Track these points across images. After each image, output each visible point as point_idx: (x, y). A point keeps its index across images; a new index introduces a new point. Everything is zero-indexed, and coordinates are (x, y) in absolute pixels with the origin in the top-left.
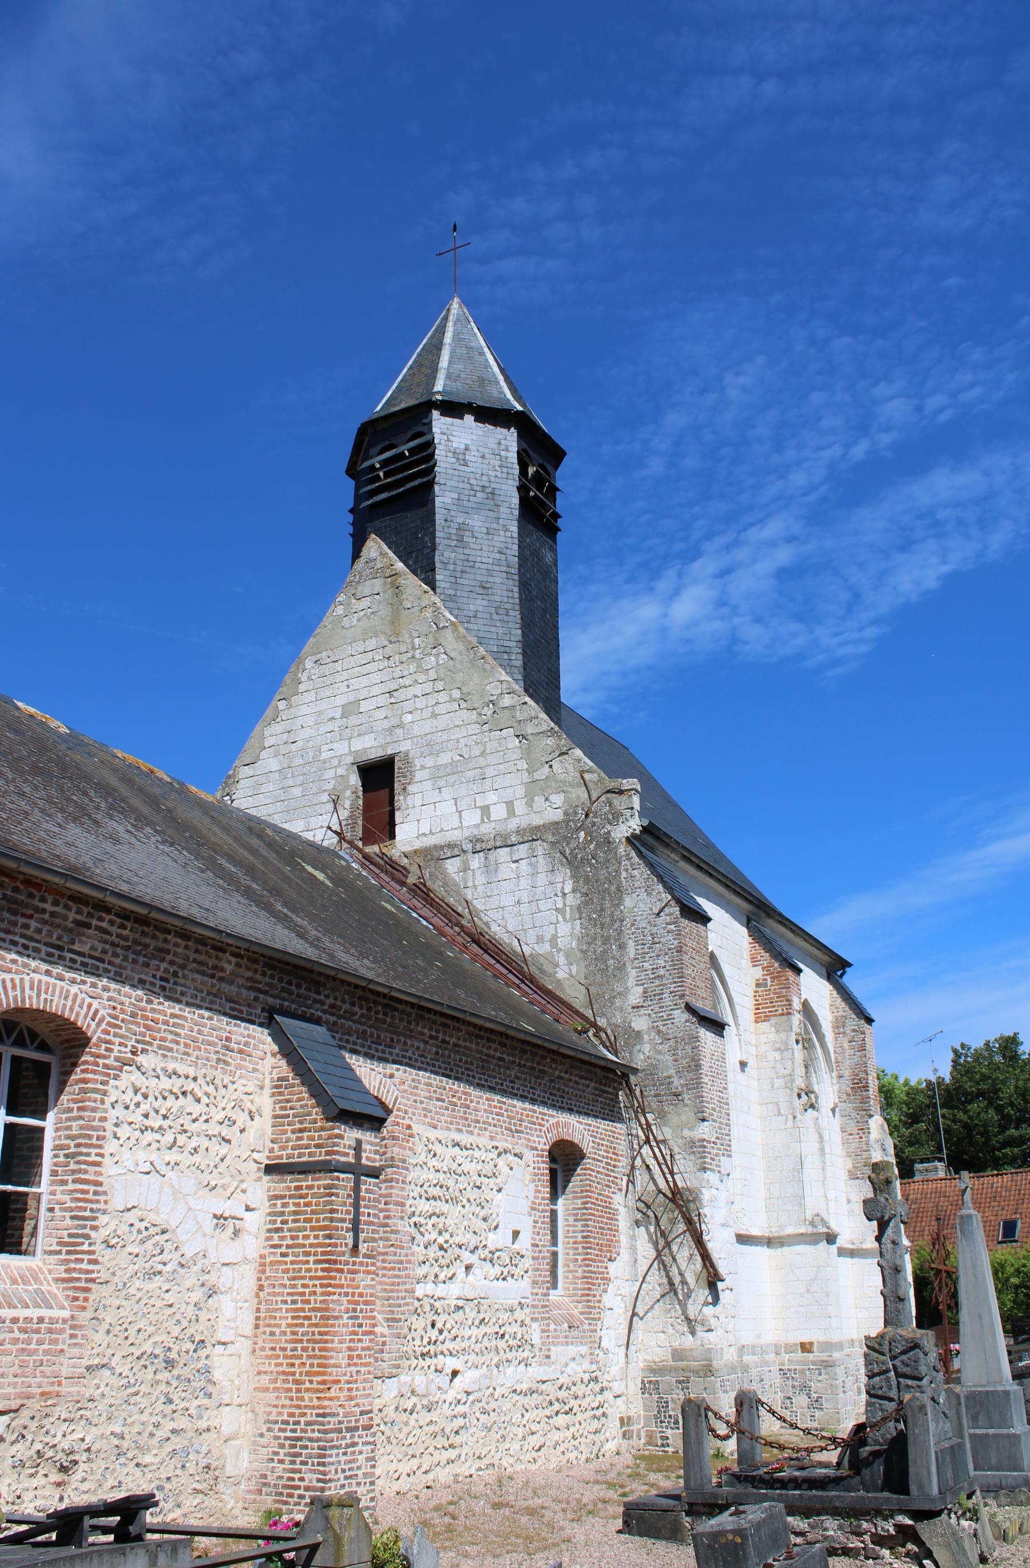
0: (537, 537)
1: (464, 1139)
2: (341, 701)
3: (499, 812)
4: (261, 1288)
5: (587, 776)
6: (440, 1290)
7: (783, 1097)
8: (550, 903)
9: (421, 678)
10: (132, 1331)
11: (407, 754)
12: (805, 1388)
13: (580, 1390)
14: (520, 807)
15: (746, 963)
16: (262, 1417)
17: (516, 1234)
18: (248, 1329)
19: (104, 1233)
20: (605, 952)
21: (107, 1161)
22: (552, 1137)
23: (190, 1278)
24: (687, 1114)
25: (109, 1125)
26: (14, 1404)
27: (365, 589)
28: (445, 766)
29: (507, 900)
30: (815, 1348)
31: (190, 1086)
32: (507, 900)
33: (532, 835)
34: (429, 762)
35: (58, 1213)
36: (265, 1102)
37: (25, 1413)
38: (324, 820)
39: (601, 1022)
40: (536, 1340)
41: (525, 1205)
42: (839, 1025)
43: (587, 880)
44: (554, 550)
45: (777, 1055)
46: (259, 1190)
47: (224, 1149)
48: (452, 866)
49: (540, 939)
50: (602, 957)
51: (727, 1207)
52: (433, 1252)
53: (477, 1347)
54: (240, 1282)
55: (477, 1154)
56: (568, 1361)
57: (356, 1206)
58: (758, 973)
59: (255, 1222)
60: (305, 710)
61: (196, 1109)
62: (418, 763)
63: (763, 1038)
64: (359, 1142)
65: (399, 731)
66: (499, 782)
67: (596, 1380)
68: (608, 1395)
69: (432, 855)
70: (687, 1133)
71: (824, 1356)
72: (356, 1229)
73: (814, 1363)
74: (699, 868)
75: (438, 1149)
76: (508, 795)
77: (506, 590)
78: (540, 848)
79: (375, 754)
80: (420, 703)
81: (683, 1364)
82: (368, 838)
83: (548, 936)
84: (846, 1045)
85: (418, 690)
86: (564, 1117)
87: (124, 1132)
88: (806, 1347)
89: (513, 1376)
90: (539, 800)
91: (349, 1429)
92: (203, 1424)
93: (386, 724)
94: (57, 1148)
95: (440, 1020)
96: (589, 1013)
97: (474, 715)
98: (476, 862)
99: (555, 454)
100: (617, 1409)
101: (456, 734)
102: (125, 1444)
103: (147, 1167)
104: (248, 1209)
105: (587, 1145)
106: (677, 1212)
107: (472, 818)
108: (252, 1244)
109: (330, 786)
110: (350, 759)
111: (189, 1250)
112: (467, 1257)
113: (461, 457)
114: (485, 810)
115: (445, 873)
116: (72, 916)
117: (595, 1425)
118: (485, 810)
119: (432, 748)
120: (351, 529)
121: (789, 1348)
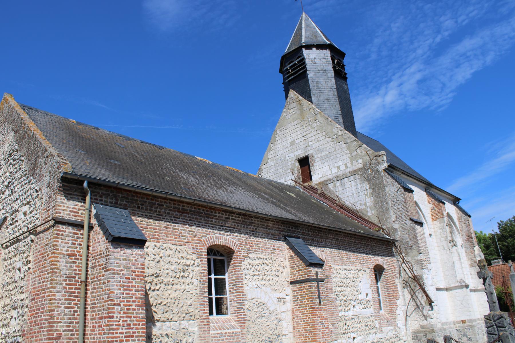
1: (347, 267)
2: (289, 141)
3: (343, 167)
4: (294, 318)
6: (346, 314)
7: (445, 243)
11: (312, 154)
12: (465, 334)
14: (349, 165)
15: (427, 203)
17: (367, 295)
19: (247, 306)
20: (382, 205)
21: (245, 285)
22: (374, 264)
23: (273, 317)
24: (415, 252)
25: (243, 275)
27: (291, 106)
29: (349, 194)
30: (467, 322)
31: (265, 261)
32: (349, 194)
33: (354, 173)
34: (319, 155)
35: (233, 302)
36: (287, 263)
39: (384, 227)
40: (377, 326)
41: (368, 286)
42: (460, 219)
43: (373, 184)
45: (441, 231)
46: (289, 289)
47: (277, 279)
50: (381, 207)
52: (343, 303)
54: (288, 316)
55: (352, 272)
57: (319, 291)
58: (431, 206)
59: (289, 299)
60: (279, 145)
61: (268, 268)
62: (316, 156)
63: (436, 226)
64: (317, 272)
67: (397, 337)
69: (325, 183)
70: (416, 258)
71: (470, 324)
72: (319, 298)
73: (467, 326)
75: (340, 271)
76: (345, 162)
77: (334, 100)
78: (357, 176)
79: (302, 155)
80: (314, 138)
82: (304, 181)
83: (363, 203)
84: (463, 225)
85: (312, 134)
86: (377, 258)
87: (248, 277)
88: (463, 322)
93: (304, 146)
94: (230, 283)
97: (330, 139)
98: (338, 184)
101: (326, 146)
103: (256, 286)
105: (385, 265)
107: (335, 170)
109: (290, 167)
110: (295, 158)
111: (271, 309)
112: (353, 303)
113: (314, 61)
114: (338, 168)
115: (329, 188)
116: (224, 216)
118: (338, 168)
119: (319, 151)
120: (284, 89)
121: (458, 322)
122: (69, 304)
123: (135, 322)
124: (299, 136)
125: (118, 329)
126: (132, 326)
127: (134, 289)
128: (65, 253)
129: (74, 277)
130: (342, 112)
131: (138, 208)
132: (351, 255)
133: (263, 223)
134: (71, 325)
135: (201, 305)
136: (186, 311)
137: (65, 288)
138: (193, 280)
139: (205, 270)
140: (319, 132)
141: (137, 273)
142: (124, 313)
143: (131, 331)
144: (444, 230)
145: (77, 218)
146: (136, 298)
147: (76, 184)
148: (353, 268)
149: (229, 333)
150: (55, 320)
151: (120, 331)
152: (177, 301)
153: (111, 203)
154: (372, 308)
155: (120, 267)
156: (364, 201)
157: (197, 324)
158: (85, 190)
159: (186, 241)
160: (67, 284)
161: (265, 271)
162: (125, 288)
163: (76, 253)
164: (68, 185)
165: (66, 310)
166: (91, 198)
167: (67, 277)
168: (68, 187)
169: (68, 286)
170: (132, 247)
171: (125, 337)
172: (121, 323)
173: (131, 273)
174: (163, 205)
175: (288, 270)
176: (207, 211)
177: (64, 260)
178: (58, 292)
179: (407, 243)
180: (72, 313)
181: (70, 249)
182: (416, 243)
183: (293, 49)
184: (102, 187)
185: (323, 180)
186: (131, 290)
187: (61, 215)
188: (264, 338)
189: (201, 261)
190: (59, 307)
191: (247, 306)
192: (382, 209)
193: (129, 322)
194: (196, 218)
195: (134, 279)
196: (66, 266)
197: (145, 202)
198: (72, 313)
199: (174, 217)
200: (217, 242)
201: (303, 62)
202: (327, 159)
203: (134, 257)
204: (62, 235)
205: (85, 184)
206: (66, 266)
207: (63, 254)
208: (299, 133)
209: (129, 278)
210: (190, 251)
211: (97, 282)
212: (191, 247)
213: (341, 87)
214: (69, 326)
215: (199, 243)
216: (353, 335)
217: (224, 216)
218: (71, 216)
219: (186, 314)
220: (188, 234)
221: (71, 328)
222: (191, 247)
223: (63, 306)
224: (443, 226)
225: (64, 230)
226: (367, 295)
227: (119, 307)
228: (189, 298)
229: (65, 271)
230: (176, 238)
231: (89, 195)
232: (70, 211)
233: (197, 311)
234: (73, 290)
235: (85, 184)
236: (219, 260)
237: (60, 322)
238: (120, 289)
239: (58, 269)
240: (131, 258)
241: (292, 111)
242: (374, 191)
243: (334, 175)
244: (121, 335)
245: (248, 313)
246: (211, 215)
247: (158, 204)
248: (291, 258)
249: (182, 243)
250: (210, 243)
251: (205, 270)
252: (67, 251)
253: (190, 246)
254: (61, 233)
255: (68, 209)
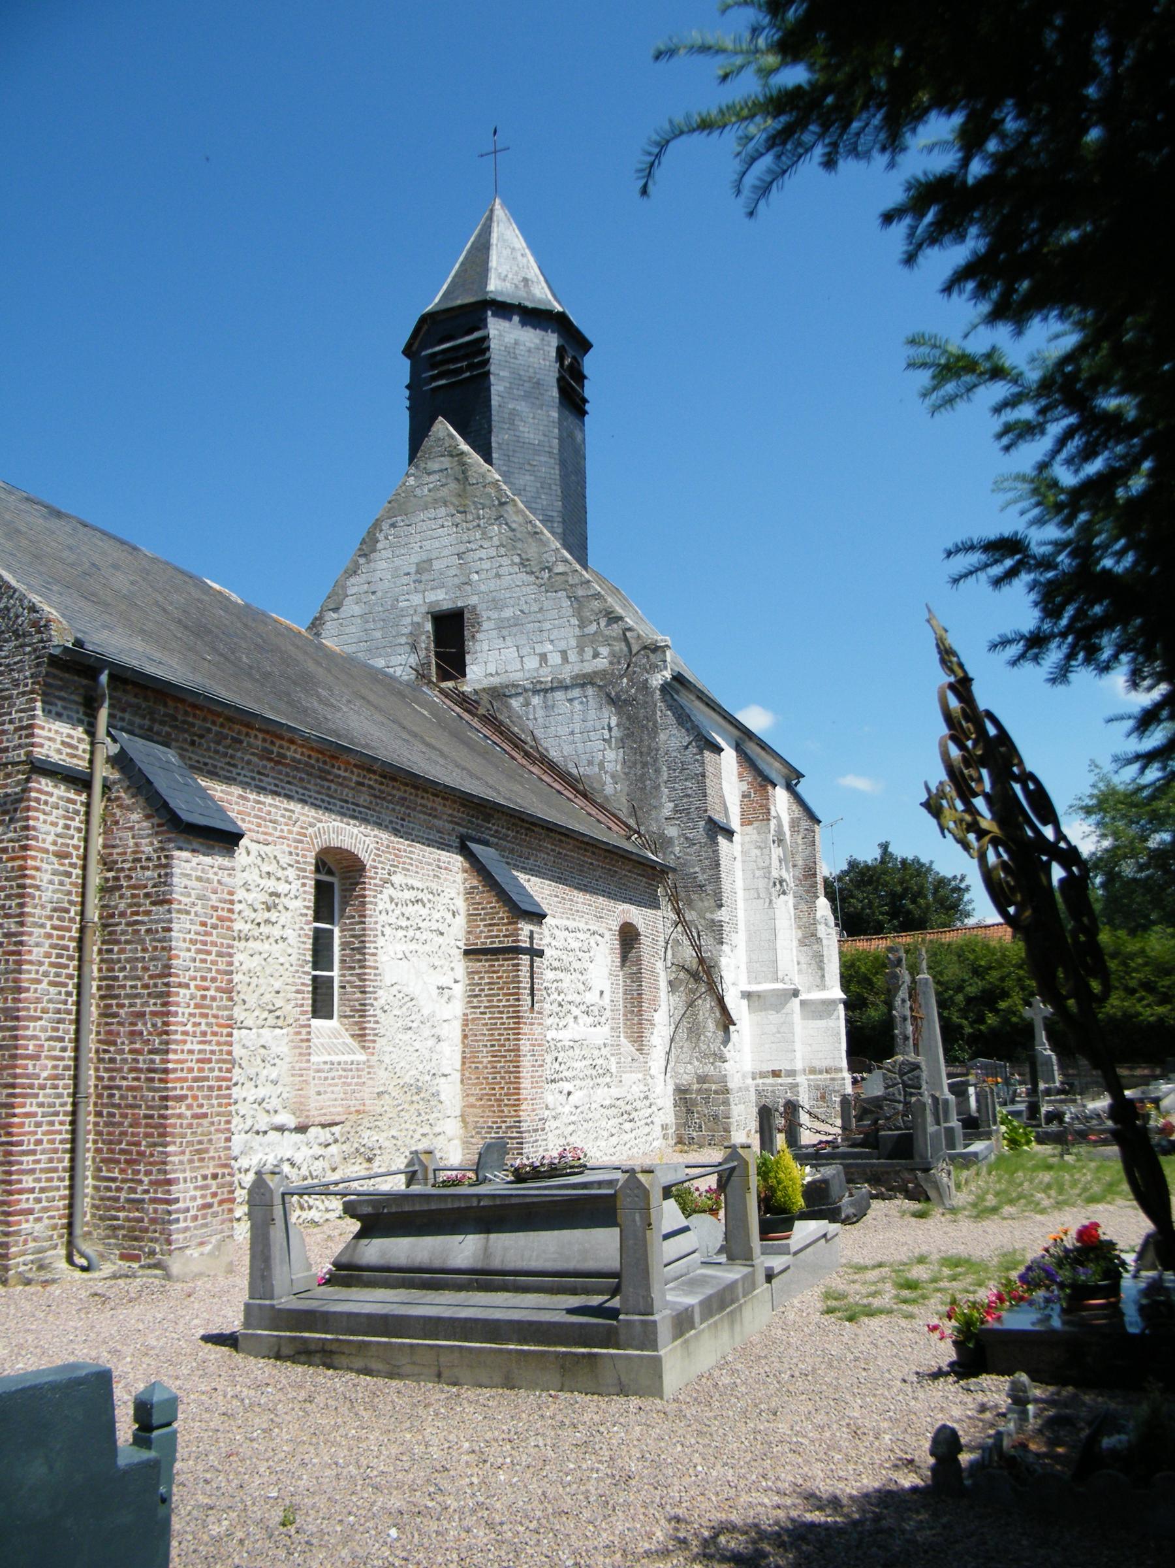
0: (571, 420)
1: (571, 924)
2: (415, 559)
3: (555, 659)
4: (465, 1036)
5: (628, 634)
6: (560, 1035)
7: (762, 884)
8: (598, 735)
9: (486, 544)
10: (398, 1067)
11: (474, 607)
13: (638, 1104)
14: (573, 656)
15: (734, 778)
16: (471, 1126)
17: (602, 993)
18: (458, 1066)
19: (382, 1001)
20: (643, 775)
21: (380, 952)
22: (621, 920)
23: (426, 1032)
24: (709, 903)
25: (379, 927)
26: (342, 1118)
27: (434, 465)
28: (508, 619)
29: (563, 730)
31: (420, 895)
32: (563, 730)
33: (584, 681)
34: (494, 615)
35: (349, 989)
36: (461, 904)
37: (348, 1124)
38: (402, 659)
39: (643, 830)
40: (614, 1070)
41: (606, 971)
42: (794, 824)
43: (629, 718)
44: (583, 431)
45: (758, 852)
46: (460, 966)
47: (440, 939)
48: (515, 703)
49: (590, 763)
50: (642, 779)
51: (735, 972)
52: (555, 1008)
53: (581, 1075)
54: (453, 1032)
55: (579, 935)
56: (631, 1085)
57: (532, 978)
58: (745, 787)
59: (459, 990)
60: (383, 565)
61: (424, 912)
62: (485, 615)
63: (747, 838)
64: (532, 932)
65: (468, 588)
66: (555, 634)
67: (646, 1098)
68: (654, 1108)
69: (499, 694)
70: (708, 915)
72: (532, 994)
74: (708, 705)
75: (556, 931)
76: (563, 645)
77: (549, 468)
78: (590, 691)
79: (447, 605)
80: (486, 565)
81: (705, 1086)
82: (444, 676)
83: (597, 761)
84: (800, 841)
85: (482, 553)
86: (626, 906)
87: (387, 930)
88: (776, 1074)
89: (603, 1095)
90: (589, 652)
91: (536, 1131)
92: (437, 1130)
93: (457, 581)
94: (342, 944)
95: (558, 837)
96: (632, 822)
97: (532, 579)
98: (536, 700)
99: (584, 345)
100: (659, 1119)
101: (518, 592)
102: (399, 1143)
103: (401, 955)
104: (456, 982)
105: (641, 928)
106: (702, 976)
107: (532, 663)
108: (457, 1008)
109: (406, 631)
110: (424, 609)
111: (426, 1012)
112: (576, 1011)
113: (511, 351)
114: (543, 657)
115: (509, 707)
116: (354, 778)
117: (647, 1129)
118: (543, 657)
119: (497, 604)
120: (407, 403)
121: (763, 1075)
122: (58, 975)
123: (215, 1029)
124: (446, 552)
125: (185, 1042)
126: (209, 1038)
127: (214, 949)
128: (52, 848)
129: (67, 911)
130: (564, 506)
131: (193, 743)
132: (580, 897)
133: (424, 802)
134: (61, 1026)
135: (298, 992)
136: (271, 1007)
137: (50, 936)
138: (288, 933)
139: (308, 908)
140: (502, 551)
141: (220, 913)
142: (197, 1006)
143: (208, 1047)
144: (766, 851)
145: (75, 761)
146: (218, 971)
147: (79, 673)
148: (582, 926)
149: (346, 1063)
150: (32, 1013)
151: (188, 1046)
152: (254, 981)
153: (141, 727)
154: (606, 1028)
155: (189, 895)
156: (600, 756)
157: (286, 1040)
158: (99, 692)
159: (278, 834)
160: (54, 928)
161: (419, 920)
162: (199, 946)
163: (71, 849)
164: (61, 675)
165: (52, 989)
166: (111, 716)
167: (55, 910)
168: (61, 679)
169: (55, 932)
170: (213, 847)
171: (198, 1061)
172: (189, 1028)
173: (210, 912)
174: (241, 742)
175: (461, 921)
176: (325, 763)
177: (49, 867)
178: (37, 945)
179: (693, 877)
180: (63, 997)
181: (60, 841)
182: (717, 879)
183: (459, 302)
184: (129, 687)
185: (495, 681)
186: (209, 953)
187: (44, 751)
188: (407, 1079)
189: (304, 885)
190: (39, 982)
191: (382, 1001)
192: (643, 782)
193: (203, 1027)
194: (302, 779)
195: (215, 927)
196: (51, 882)
197: (209, 730)
198: (63, 997)
199: (259, 773)
200: (335, 843)
201: (481, 347)
202: (514, 629)
203: (216, 874)
204: (46, 803)
205: (104, 678)
206: (51, 882)
207: (47, 851)
208: (446, 541)
209: (204, 924)
210: (285, 860)
211: (122, 927)
212: (287, 849)
213: (571, 436)
214: (57, 1030)
215: (301, 842)
216: (567, 1086)
217: (354, 778)
218: (63, 757)
219: (271, 1012)
220: (283, 816)
221: (60, 1034)
222: (287, 849)
223: (46, 980)
224: (765, 841)
225: (50, 789)
226: (602, 993)
227: (187, 992)
228: (277, 975)
229: (49, 894)
230: (259, 825)
231: (106, 705)
232: (63, 743)
233: (289, 1007)
234: (66, 943)
235: (104, 678)
236: (337, 884)
237: (41, 1018)
238: (189, 950)
239: (38, 888)
240: (211, 876)
241: (433, 478)
242: (628, 736)
243: (527, 675)
244: (190, 1057)
245: (381, 1016)
246: (329, 773)
247: (233, 738)
248: (470, 892)
249: (270, 839)
250: (319, 843)
251: (308, 908)
252: (55, 843)
253: (285, 847)
254: (43, 797)
255: (59, 739)
